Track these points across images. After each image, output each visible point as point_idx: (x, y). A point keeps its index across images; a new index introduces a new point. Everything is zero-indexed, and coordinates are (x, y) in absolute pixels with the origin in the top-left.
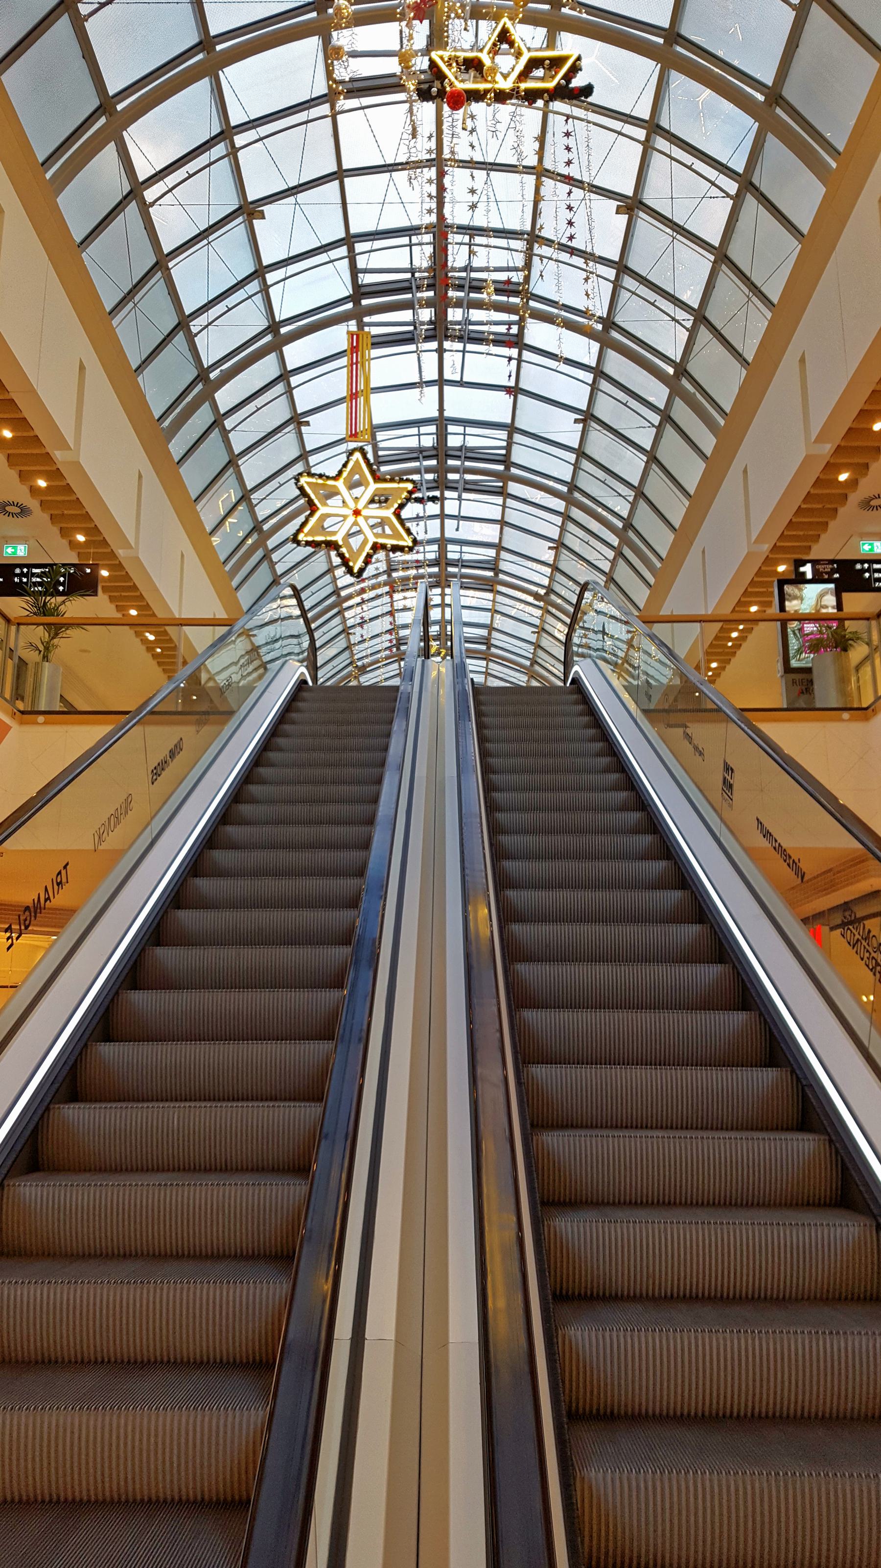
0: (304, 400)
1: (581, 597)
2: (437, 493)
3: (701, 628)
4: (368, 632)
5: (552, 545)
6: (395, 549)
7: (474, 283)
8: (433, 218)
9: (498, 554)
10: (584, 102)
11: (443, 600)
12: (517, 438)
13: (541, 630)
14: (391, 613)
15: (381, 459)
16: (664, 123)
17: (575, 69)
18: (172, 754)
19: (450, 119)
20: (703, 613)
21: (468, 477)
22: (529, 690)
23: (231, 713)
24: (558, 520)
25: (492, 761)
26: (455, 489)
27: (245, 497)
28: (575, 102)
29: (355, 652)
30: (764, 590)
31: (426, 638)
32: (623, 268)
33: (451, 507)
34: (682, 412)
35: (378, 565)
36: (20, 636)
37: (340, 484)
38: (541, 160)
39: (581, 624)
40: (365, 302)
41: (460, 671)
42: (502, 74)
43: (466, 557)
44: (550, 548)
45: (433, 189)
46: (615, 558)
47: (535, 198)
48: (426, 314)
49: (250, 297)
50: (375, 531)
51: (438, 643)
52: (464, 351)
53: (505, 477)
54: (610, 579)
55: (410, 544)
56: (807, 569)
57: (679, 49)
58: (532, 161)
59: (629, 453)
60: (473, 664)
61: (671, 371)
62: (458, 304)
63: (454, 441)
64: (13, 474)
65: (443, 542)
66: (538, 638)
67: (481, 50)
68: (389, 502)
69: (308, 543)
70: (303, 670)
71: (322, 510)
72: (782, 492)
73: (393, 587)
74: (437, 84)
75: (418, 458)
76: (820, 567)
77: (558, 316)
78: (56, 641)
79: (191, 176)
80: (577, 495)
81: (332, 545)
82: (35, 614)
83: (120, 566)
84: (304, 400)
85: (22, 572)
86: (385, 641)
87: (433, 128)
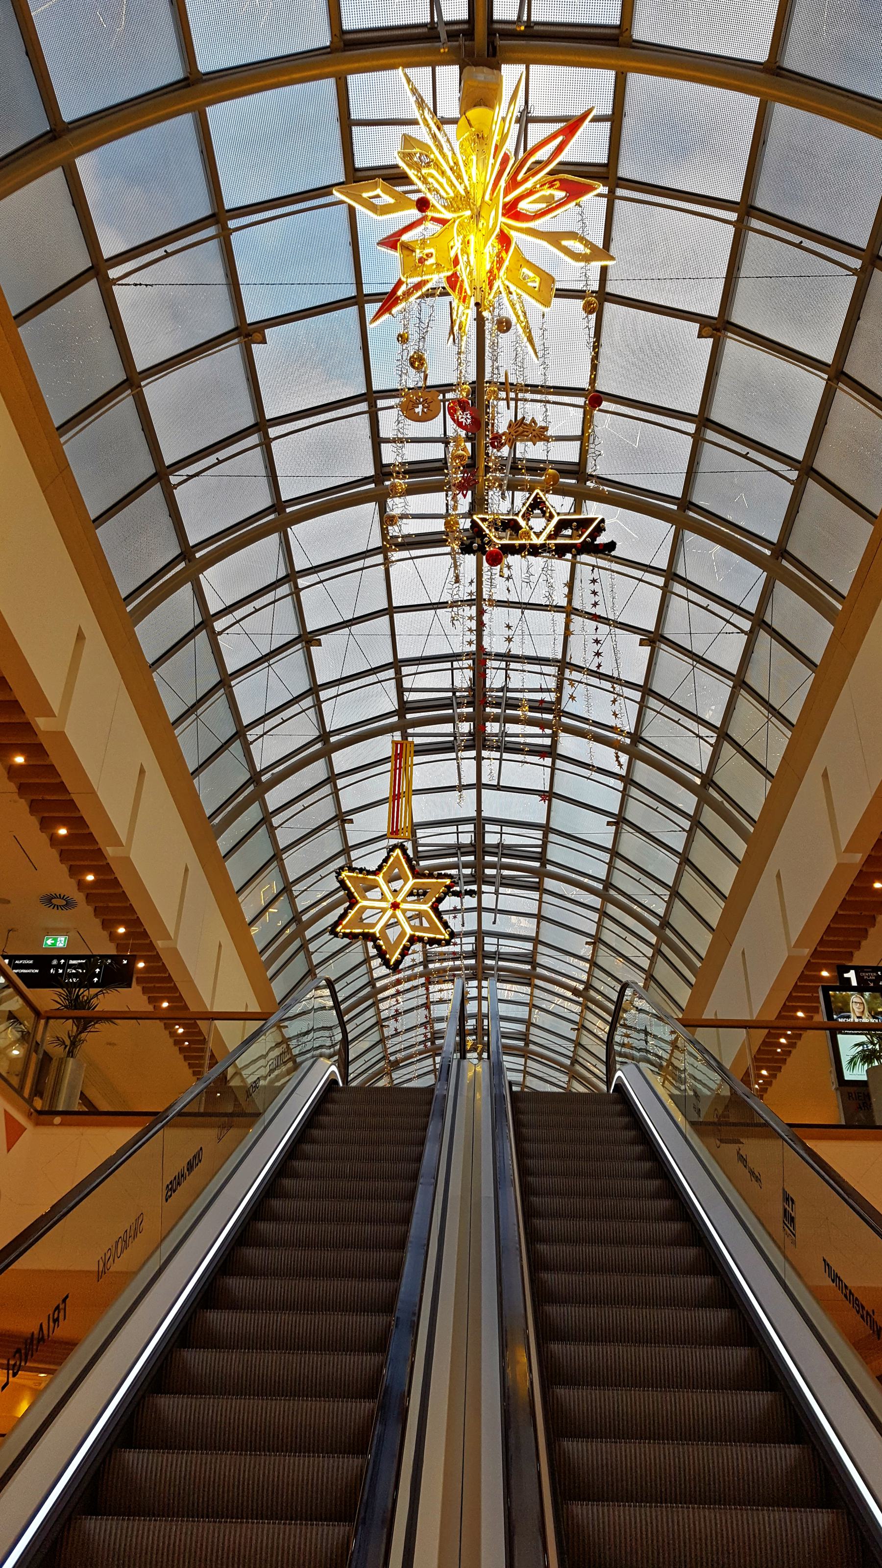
0: (348, 801)
1: (621, 994)
2: (474, 887)
3: (748, 1033)
4: (402, 1025)
5: (589, 940)
6: (432, 942)
7: (510, 702)
8: (473, 648)
9: (535, 948)
10: (608, 555)
11: (480, 992)
12: (552, 837)
13: (581, 1027)
14: (427, 1006)
15: (420, 855)
16: (681, 572)
17: (600, 529)
18: (190, 1166)
19: (489, 573)
20: (749, 1018)
21: (505, 872)
22: (568, 1097)
23: (258, 1115)
24: (595, 916)
25: (531, 1163)
26: (492, 883)
27: (287, 889)
28: (600, 555)
29: (388, 1046)
30: (810, 995)
31: (462, 1033)
32: (648, 691)
33: (488, 901)
34: (709, 817)
35: (415, 956)
36: (48, 1028)
37: (380, 879)
38: (570, 601)
39: (622, 1022)
40: (409, 716)
41: (497, 1070)
42: (535, 533)
43: (503, 950)
44: (587, 943)
45: (473, 625)
46: (653, 956)
47: (565, 633)
48: (465, 727)
49: (304, 711)
50: (412, 923)
51: (474, 1037)
52: (501, 760)
53: (541, 874)
54: (650, 977)
55: (447, 937)
56: (851, 975)
57: (691, 514)
58: (563, 602)
59: (662, 855)
60: (509, 1061)
61: (698, 781)
62: (496, 719)
63: (491, 839)
64: (64, 868)
65: (479, 935)
66: (578, 1036)
67: (517, 514)
68: (428, 895)
69: (345, 935)
70: (334, 1068)
71: (363, 903)
72: (816, 901)
73: (430, 979)
74: (478, 540)
75: (457, 854)
76: (865, 975)
77: (590, 731)
78: (83, 1035)
79: (257, 611)
80: (612, 892)
81: (372, 937)
82: (66, 1007)
83: (158, 957)
84: (348, 801)
85: (59, 963)
86: (418, 1035)
87: (474, 575)
